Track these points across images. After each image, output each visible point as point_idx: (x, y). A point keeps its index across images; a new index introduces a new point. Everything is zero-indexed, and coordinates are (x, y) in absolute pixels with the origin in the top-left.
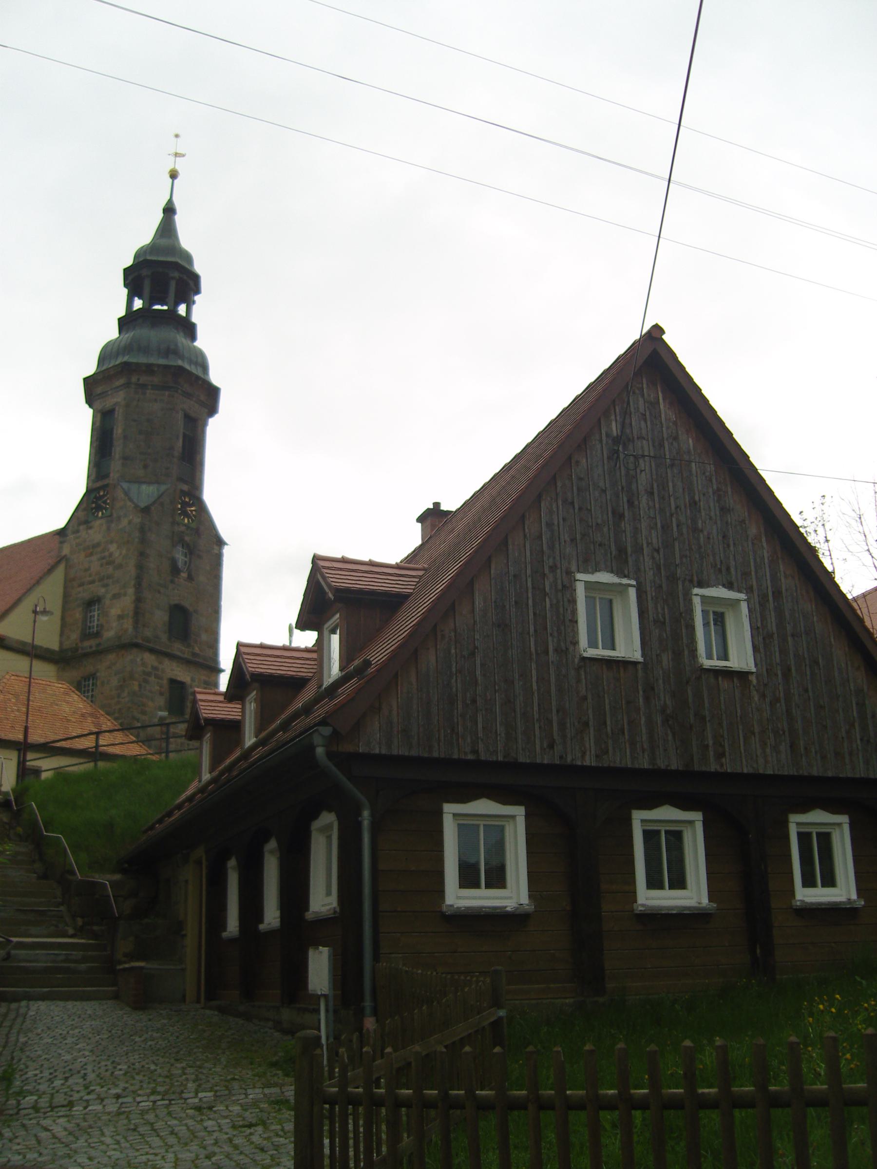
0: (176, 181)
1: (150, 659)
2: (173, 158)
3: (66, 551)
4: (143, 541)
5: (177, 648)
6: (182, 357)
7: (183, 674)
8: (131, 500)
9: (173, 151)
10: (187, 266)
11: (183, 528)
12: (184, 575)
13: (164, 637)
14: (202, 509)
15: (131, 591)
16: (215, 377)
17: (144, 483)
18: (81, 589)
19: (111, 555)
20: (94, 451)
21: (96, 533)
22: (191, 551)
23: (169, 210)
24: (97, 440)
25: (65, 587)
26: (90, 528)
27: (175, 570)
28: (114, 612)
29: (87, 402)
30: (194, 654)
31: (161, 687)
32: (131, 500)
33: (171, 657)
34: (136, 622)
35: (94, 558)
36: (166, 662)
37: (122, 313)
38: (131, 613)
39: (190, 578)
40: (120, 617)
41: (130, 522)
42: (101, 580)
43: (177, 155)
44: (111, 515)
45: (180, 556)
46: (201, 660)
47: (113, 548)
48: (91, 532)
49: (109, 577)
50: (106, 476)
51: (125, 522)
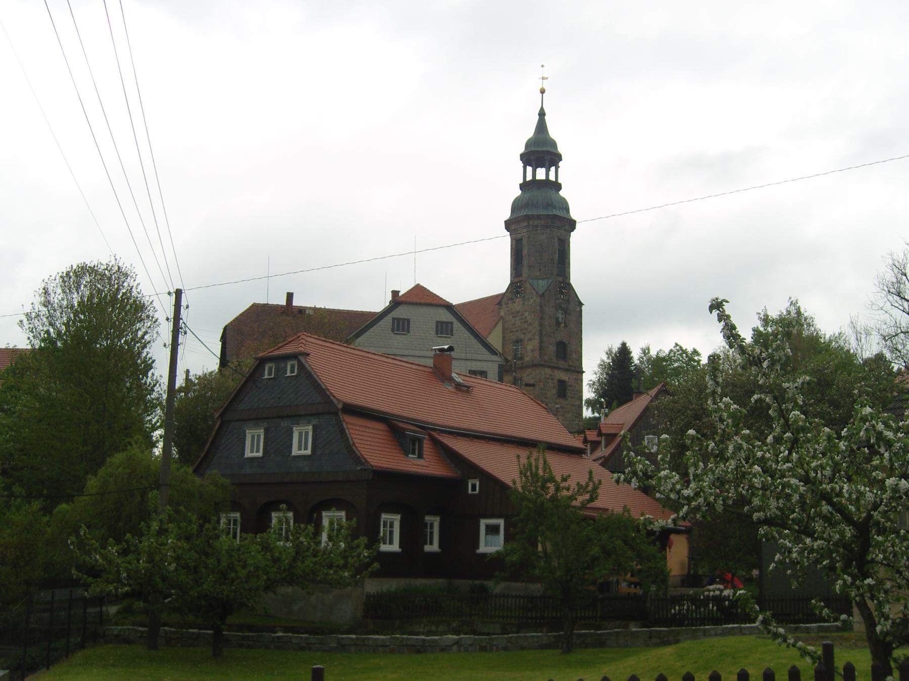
0: (544, 94)
1: (548, 371)
2: (541, 80)
3: (502, 313)
4: (542, 311)
5: (561, 363)
6: (554, 207)
7: (564, 376)
8: (534, 289)
9: (541, 76)
10: (554, 151)
11: (561, 301)
12: (563, 325)
13: (554, 359)
14: (570, 285)
15: (537, 337)
16: (574, 214)
17: (540, 279)
18: (511, 334)
19: (526, 318)
20: (512, 261)
21: (517, 305)
22: (566, 312)
23: (542, 114)
24: (514, 255)
25: (503, 333)
26: (514, 302)
27: (558, 324)
28: (529, 347)
29: (506, 229)
30: (570, 366)
31: (554, 383)
32: (534, 289)
33: (558, 368)
34: (541, 353)
35: (517, 319)
36: (556, 371)
37: (521, 181)
38: (538, 348)
39: (566, 326)
40: (532, 351)
41: (534, 301)
42: (521, 330)
43: (543, 78)
44: (524, 297)
45: (560, 316)
46: (573, 368)
47: (526, 314)
48: (515, 305)
49: (526, 329)
50: (521, 275)
51: (532, 301)
